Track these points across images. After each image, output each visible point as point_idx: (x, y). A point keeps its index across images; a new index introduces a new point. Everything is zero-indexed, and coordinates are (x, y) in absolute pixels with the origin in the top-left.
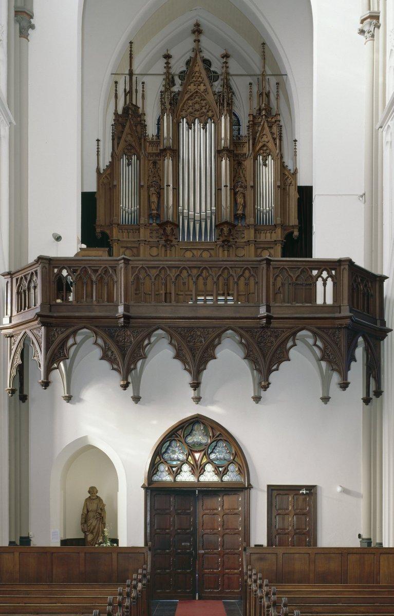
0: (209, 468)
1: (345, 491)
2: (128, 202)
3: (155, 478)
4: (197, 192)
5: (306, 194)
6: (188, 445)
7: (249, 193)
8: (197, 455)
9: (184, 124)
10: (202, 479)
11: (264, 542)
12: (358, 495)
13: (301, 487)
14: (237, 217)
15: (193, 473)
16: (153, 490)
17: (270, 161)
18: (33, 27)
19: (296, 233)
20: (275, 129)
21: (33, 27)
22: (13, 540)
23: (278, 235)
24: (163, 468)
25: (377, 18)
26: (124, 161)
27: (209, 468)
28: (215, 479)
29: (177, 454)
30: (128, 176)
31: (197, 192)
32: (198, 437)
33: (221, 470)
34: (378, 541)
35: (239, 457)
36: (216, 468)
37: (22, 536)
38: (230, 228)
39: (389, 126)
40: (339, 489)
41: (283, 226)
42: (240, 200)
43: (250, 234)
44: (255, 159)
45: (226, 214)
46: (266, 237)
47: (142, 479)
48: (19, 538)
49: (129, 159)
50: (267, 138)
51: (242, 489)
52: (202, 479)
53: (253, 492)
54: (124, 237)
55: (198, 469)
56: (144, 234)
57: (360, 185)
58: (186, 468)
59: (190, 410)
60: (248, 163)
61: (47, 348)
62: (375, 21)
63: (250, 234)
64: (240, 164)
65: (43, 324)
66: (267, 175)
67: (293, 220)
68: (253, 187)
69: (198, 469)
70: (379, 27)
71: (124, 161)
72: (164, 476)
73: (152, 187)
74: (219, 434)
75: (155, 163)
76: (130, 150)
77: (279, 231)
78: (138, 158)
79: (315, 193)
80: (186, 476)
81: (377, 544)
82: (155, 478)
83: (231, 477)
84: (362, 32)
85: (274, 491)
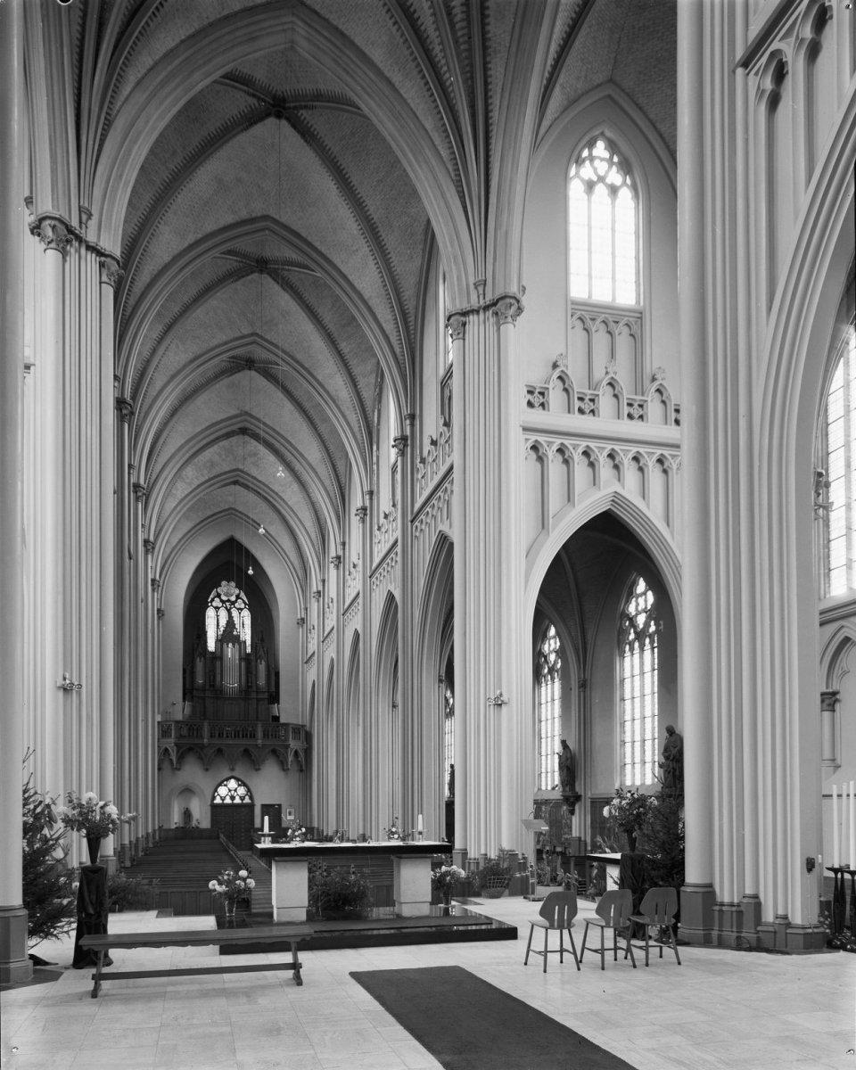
3: (215, 802)
17: (263, 662)
23: (266, 695)
28: (240, 802)
46: (261, 696)
50: (261, 653)
56: (208, 694)
66: (262, 667)
67: (273, 689)
72: (218, 801)
80: (228, 801)
82: (215, 802)
83: (247, 800)
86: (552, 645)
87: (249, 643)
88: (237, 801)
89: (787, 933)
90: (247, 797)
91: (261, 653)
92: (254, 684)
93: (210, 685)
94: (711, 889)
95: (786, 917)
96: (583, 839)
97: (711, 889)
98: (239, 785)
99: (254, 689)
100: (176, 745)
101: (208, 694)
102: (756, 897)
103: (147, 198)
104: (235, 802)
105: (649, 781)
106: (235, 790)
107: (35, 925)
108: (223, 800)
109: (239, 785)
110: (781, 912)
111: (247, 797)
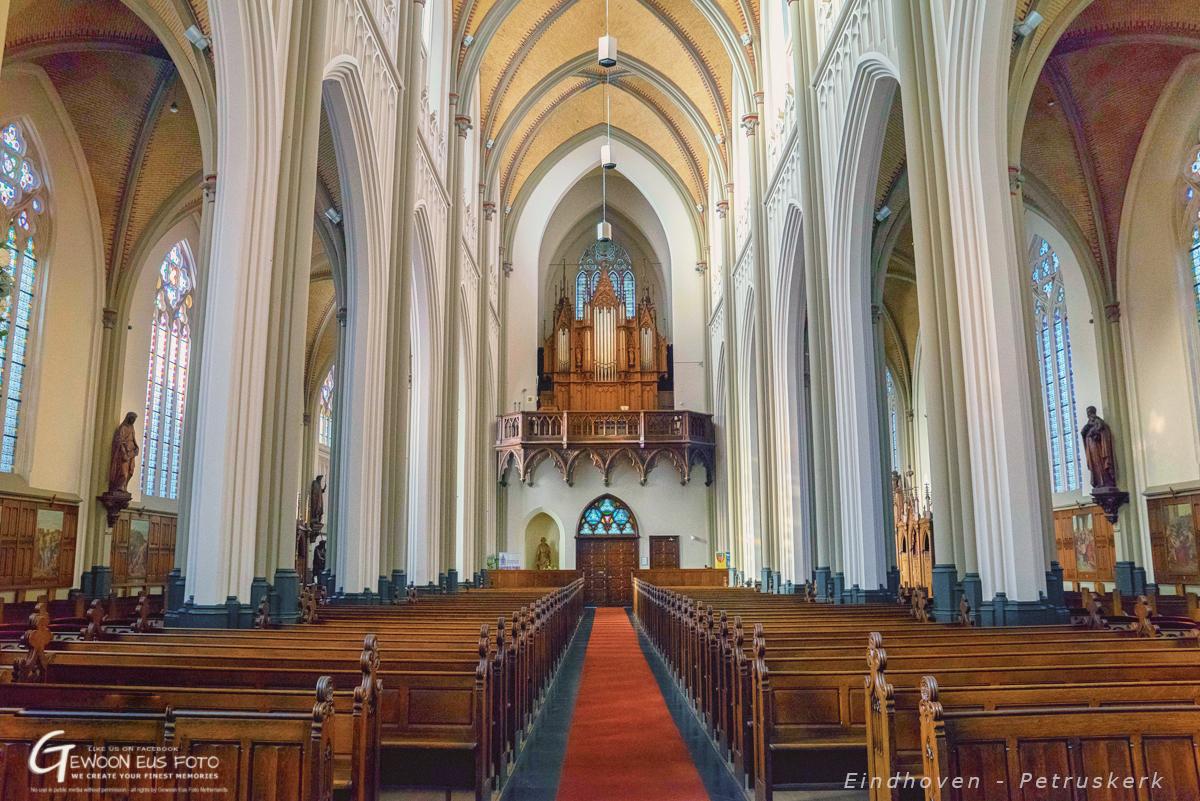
0: (614, 525)
1: (697, 539)
2: (563, 354)
3: (582, 532)
4: (605, 344)
5: (670, 349)
6: (601, 512)
7: (637, 351)
8: (607, 518)
9: (596, 310)
10: (610, 532)
11: (648, 567)
12: (705, 542)
13: (669, 537)
14: (630, 366)
15: (605, 529)
16: (581, 540)
17: (649, 331)
18: (511, 270)
19: (666, 376)
20: (652, 312)
21: (511, 270)
22: (261, 575)
23: (655, 378)
24: (586, 526)
25: (757, 118)
26: (561, 332)
27: (614, 525)
28: (618, 532)
29: (594, 516)
30: (563, 339)
31: (605, 344)
32: (607, 506)
33: (621, 527)
34: (969, 570)
35: (631, 518)
36: (619, 525)
37: (281, 567)
38: (626, 375)
39: (846, 35)
40: (692, 538)
41: (659, 372)
42: (631, 356)
43: (637, 377)
44: (640, 330)
45: (623, 366)
46: (647, 379)
47: (574, 533)
48: (273, 572)
49: (564, 331)
50: (647, 318)
51: (634, 539)
52: (610, 532)
53: (640, 540)
54: (561, 379)
55: (607, 526)
56: (573, 378)
57: (701, 358)
58: (600, 526)
59: (602, 490)
60: (636, 333)
61: (525, 459)
62: (754, 120)
63: (637, 377)
64: (631, 333)
65: (523, 447)
66: (648, 339)
67: (664, 368)
68: (640, 348)
69: (607, 526)
70: (758, 124)
71: (561, 332)
72: (586, 531)
73: (578, 348)
74: (620, 504)
75: (579, 334)
76: (564, 326)
77: (656, 374)
78: (569, 331)
79: (674, 348)
80: (600, 531)
81: (967, 575)
82: (582, 532)
83: (628, 530)
84: (698, 270)
85: (655, 541)
86: (29, 469)
87: (329, 376)
88: (614, 531)
89: (1004, 611)
90: (628, 525)
91: (647, 318)
92: (637, 362)
93: (577, 367)
94: (976, 579)
95: (857, 586)
96: (1137, 565)
97: (976, 579)
98: (616, 508)
99: (638, 369)
100: (524, 446)
101: (573, 378)
102: (976, 575)
103: (110, 219)
104: (596, 532)
105: (173, 496)
106: (611, 515)
107: (219, 779)
108: (593, 530)
109: (616, 508)
110: (854, 583)
111: (628, 525)
